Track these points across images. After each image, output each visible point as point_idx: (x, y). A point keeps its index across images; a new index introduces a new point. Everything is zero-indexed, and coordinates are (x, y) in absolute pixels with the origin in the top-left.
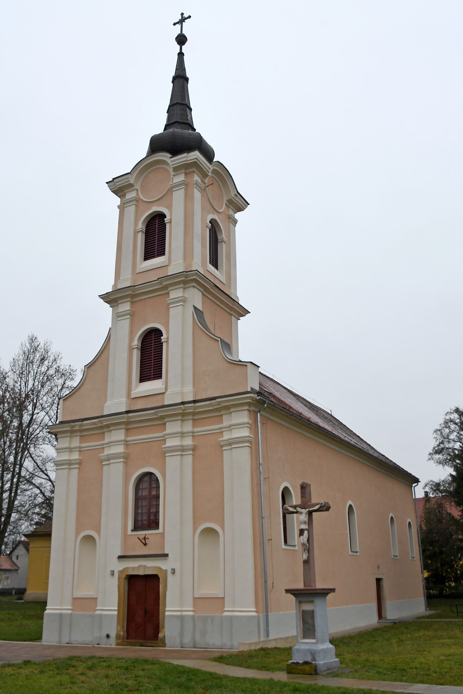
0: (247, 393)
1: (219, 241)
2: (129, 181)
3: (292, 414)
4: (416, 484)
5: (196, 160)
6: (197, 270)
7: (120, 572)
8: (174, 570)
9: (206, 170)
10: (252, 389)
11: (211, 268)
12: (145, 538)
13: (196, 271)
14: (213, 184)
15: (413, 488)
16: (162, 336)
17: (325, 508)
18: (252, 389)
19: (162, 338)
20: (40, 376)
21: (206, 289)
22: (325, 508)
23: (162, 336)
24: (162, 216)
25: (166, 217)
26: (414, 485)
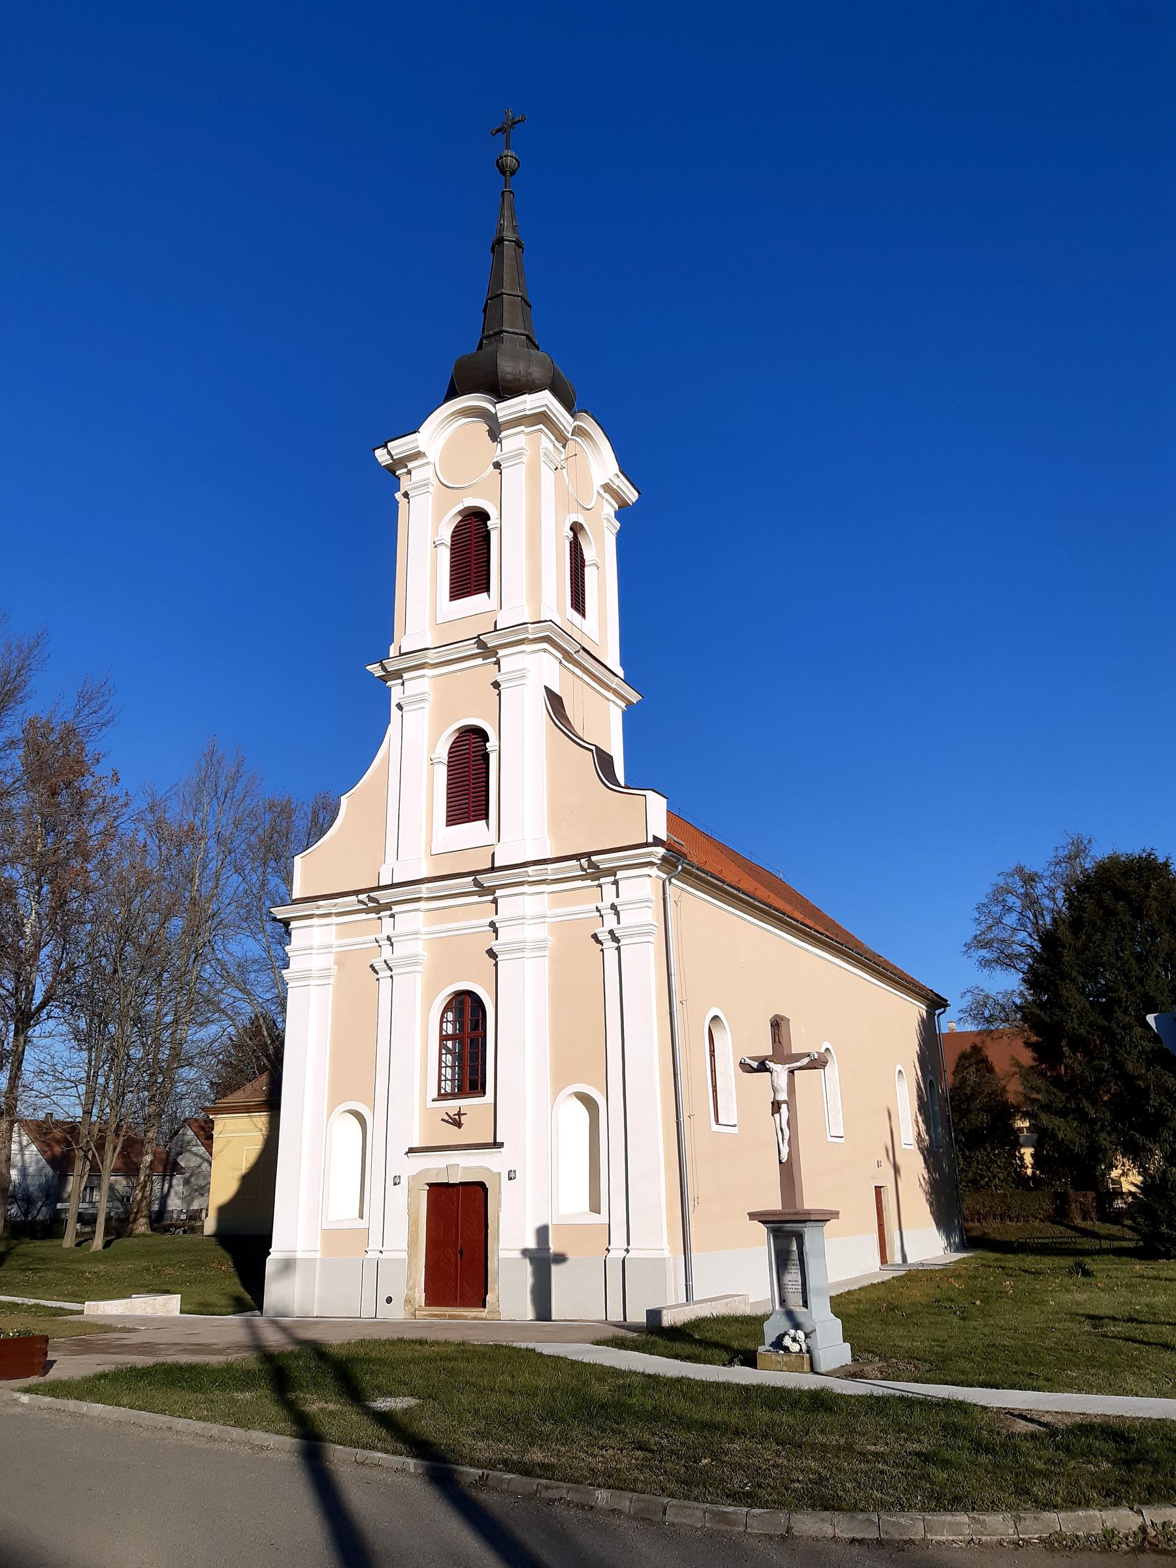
0: (646, 845)
1: (586, 564)
2: (417, 447)
3: (459, 1252)
4: (943, 1009)
5: (545, 409)
6: (551, 621)
7: (413, 1179)
8: (510, 1179)
9: (563, 429)
10: (655, 837)
11: (576, 616)
12: (459, 1114)
13: (550, 623)
14: (576, 455)
15: (936, 1017)
16: (488, 741)
17: (817, 1063)
18: (655, 837)
19: (488, 745)
20: (1068, 1237)
21: (567, 655)
22: (817, 1063)
23: (488, 741)
24: (483, 516)
25: (489, 519)
26: (937, 1012)
